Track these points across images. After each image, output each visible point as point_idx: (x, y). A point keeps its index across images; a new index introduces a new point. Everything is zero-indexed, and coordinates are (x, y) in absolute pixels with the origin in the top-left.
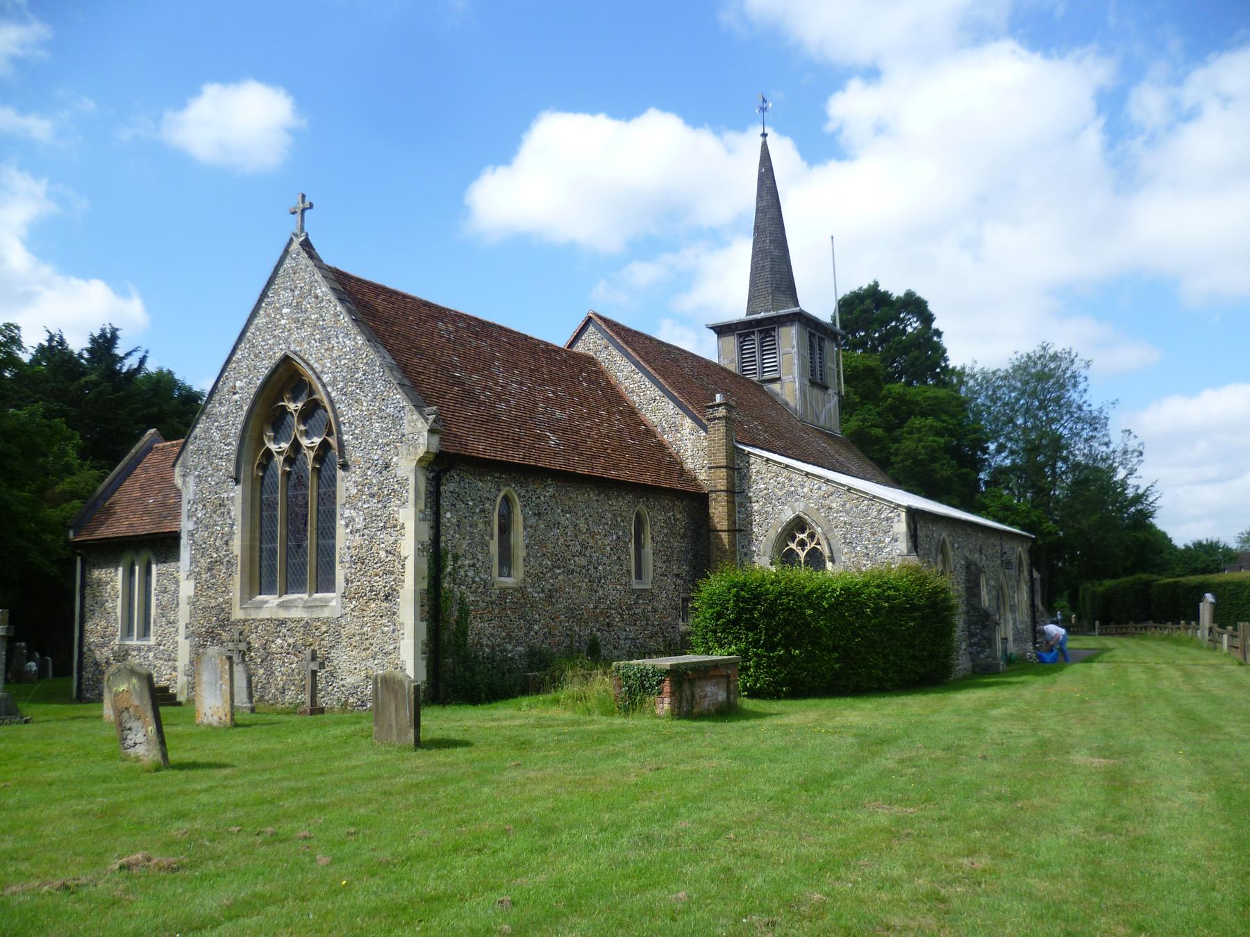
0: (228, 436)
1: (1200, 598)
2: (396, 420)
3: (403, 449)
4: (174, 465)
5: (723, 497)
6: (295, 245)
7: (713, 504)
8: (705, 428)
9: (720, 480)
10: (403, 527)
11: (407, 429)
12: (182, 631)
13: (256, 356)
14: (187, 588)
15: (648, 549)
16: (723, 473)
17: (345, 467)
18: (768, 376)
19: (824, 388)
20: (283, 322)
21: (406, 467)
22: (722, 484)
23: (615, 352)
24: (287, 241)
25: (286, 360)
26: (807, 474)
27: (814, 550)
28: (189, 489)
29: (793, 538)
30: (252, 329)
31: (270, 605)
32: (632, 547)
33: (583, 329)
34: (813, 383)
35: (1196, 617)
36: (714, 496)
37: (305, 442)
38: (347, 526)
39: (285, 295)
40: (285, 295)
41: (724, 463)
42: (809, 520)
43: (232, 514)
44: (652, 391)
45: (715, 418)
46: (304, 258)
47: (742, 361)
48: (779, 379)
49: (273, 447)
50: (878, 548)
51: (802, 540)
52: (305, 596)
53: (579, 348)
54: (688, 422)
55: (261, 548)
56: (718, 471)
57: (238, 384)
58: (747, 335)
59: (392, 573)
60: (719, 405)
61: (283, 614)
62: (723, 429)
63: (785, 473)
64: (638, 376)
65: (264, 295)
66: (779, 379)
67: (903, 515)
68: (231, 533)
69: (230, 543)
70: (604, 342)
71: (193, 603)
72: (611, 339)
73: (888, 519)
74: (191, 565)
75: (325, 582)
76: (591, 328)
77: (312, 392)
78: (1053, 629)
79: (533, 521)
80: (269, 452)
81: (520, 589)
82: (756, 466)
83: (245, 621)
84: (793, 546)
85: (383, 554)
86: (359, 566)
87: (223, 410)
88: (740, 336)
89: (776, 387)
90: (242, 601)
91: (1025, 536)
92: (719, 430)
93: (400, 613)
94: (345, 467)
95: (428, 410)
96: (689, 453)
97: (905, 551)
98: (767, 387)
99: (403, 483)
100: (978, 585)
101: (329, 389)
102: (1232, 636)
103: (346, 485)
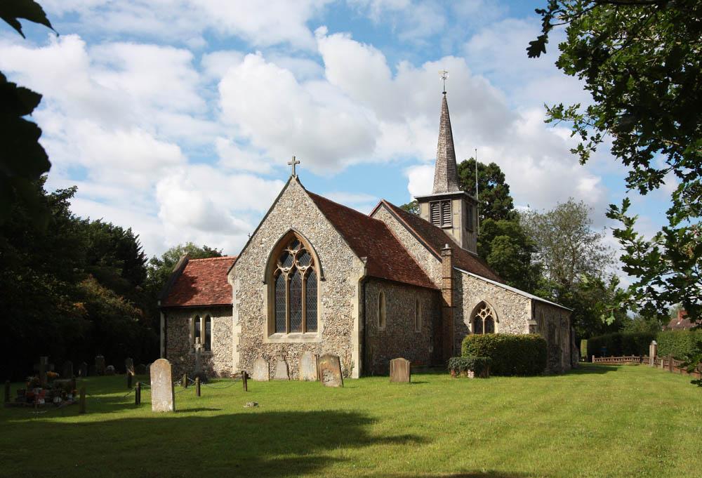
0: (259, 263)
1: (650, 343)
2: (349, 262)
3: (352, 274)
4: (228, 274)
5: (449, 292)
6: (294, 180)
7: (444, 295)
8: (441, 260)
9: (448, 283)
10: (352, 306)
11: (354, 266)
12: (235, 349)
13: (273, 228)
14: (237, 330)
15: (420, 315)
16: (449, 281)
17: (323, 280)
18: (445, 226)
19: (471, 232)
20: (287, 214)
21: (354, 281)
22: (449, 286)
23: (395, 220)
24: (289, 178)
25: (291, 231)
26: (487, 283)
27: (489, 317)
28: (236, 285)
29: (479, 312)
30: (270, 215)
31: (283, 337)
32: (415, 313)
33: (378, 208)
34: (467, 230)
35: (648, 353)
36: (445, 291)
37: (299, 268)
38: (324, 304)
39: (288, 203)
40: (288, 203)
41: (450, 276)
42: (488, 304)
43: (262, 297)
44: (414, 241)
45: (446, 255)
46: (298, 187)
47: (432, 217)
48: (452, 227)
49: (283, 269)
50: (519, 317)
51: (484, 312)
52: (302, 333)
53: (376, 217)
54: (431, 256)
55: (276, 313)
56: (447, 280)
57: (263, 240)
58: (436, 203)
59: (347, 324)
60: (448, 250)
61: (291, 341)
62: (449, 261)
63: (477, 281)
64: (407, 232)
65: (277, 201)
66: (452, 227)
67: (530, 302)
68: (262, 306)
69: (261, 310)
70: (389, 215)
71: (241, 336)
72: (392, 214)
73: (523, 304)
74: (239, 319)
75: (311, 325)
76: (382, 207)
77: (302, 246)
78: (653, 140)
79: (388, 303)
80: (280, 270)
81: (385, 332)
82: (465, 277)
83: (270, 344)
84: (480, 315)
85: (343, 317)
86: (331, 321)
87: (256, 251)
88: (431, 203)
89: (450, 231)
90: (269, 335)
91: (562, 308)
92: (447, 261)
93: (352, 341)
94: (323, 280)
95: (363, 258)
96: (431, 271)
97: (530, 318)
98: (445, 230)
99: (353, 288)
100: (554, 333)
101: (314, 246)
102: (665, 360)
103: (322, 288)
